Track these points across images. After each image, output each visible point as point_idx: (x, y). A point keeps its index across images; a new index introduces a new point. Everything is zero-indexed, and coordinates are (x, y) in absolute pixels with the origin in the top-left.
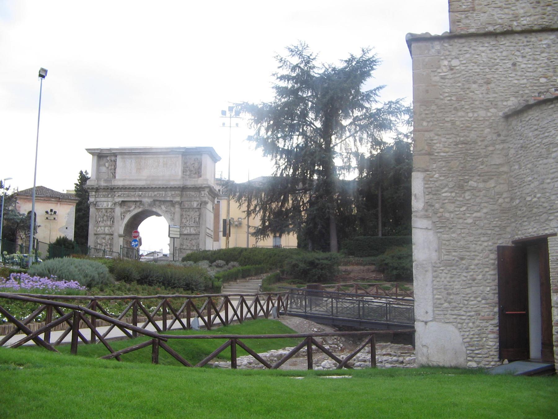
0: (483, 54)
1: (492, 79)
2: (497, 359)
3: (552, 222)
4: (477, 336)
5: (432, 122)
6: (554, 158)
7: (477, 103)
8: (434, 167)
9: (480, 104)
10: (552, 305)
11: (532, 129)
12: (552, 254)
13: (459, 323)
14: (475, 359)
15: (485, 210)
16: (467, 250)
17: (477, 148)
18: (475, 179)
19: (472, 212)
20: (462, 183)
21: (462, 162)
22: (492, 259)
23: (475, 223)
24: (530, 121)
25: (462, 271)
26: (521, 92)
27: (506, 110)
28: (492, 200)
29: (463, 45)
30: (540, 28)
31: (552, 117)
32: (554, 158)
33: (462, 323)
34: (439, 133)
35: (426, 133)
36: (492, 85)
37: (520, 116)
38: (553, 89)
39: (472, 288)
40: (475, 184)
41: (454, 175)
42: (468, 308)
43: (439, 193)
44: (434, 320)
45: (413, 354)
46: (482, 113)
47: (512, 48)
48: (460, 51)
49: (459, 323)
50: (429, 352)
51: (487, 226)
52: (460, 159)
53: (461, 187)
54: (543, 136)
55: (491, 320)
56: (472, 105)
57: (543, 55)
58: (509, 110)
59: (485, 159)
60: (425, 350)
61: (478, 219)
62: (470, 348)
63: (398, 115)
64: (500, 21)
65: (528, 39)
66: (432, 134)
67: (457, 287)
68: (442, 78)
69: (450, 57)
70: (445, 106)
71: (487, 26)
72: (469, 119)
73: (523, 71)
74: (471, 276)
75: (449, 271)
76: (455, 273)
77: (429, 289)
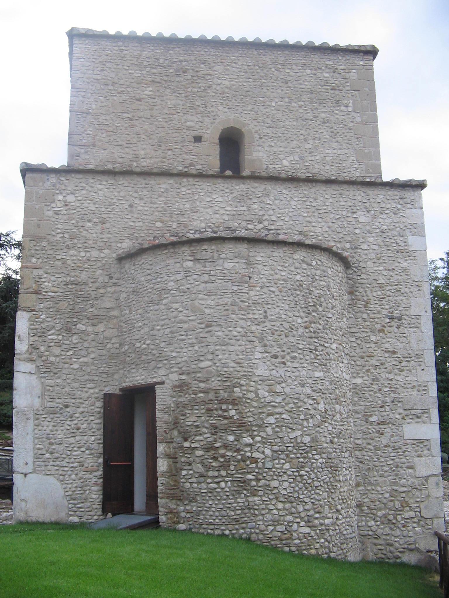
0: (100, 192)
1: (108, 219)
2: (100, 513)
3: (160, 370)
4: (80, 489)
5: (43, 260)
6: (165, 305)
7: (90, 242)
8: (41, 307)
9: (94, 243)
10: (158, 455)
11: (145, 274)
12: (159, 403)
13: (61, 475)
14: (77, 513)
15: (92, 356)
16: (73, 397)
17: (88, 289)
18: (84, 322)
19: (79, 357)
20: (70, 325)
21: (71, 303)
22: (98, 407)
23: (81, 369)
24: (143, 266)
25: (65, 419)
26: (136, 235)
27: (120, 252)
28: (100, 345)
29: (80, 180)
30: (160, 172)
31: (165, 263)
32: (165, 305)
33: (64, 475)
34: (49, 271)
35: (35, 270)
36: (108, 225)
37: (133, 259)
38: (168, 235)
39: (76, 437)
40: (83, 328)
41: (61, 317)
42: (70, 458)
43: (45, 335)
44: (34, 471)
45: (11, 509)
46: (95, 253)
47: (130, 189)
48: (76, 186)
49: (61, 475)
50: (28, 506)
51: (94, 372)
52: (69, 300)
53: (69, 330)
54: (155, 281)
55: (96, 471)
56: (85, 245)
57: (161, 199)
58: (122, 253)
59: (96, 302)
60: (23, 504)
61: (84, 364)
62: (72, 502)
63: (8, 249)
64: (120, 160)
65: (146, 181)
66: (41, 272)
67: (59, 436)
68: (56, 214)
69: (66, 191)
70: (57, 243)
71: (106, 163)
72: (81, 258)
73: (139, 214)
74: (75, 424)
75: (52, 419)
76: (58, 421)
77: (30, 438)
